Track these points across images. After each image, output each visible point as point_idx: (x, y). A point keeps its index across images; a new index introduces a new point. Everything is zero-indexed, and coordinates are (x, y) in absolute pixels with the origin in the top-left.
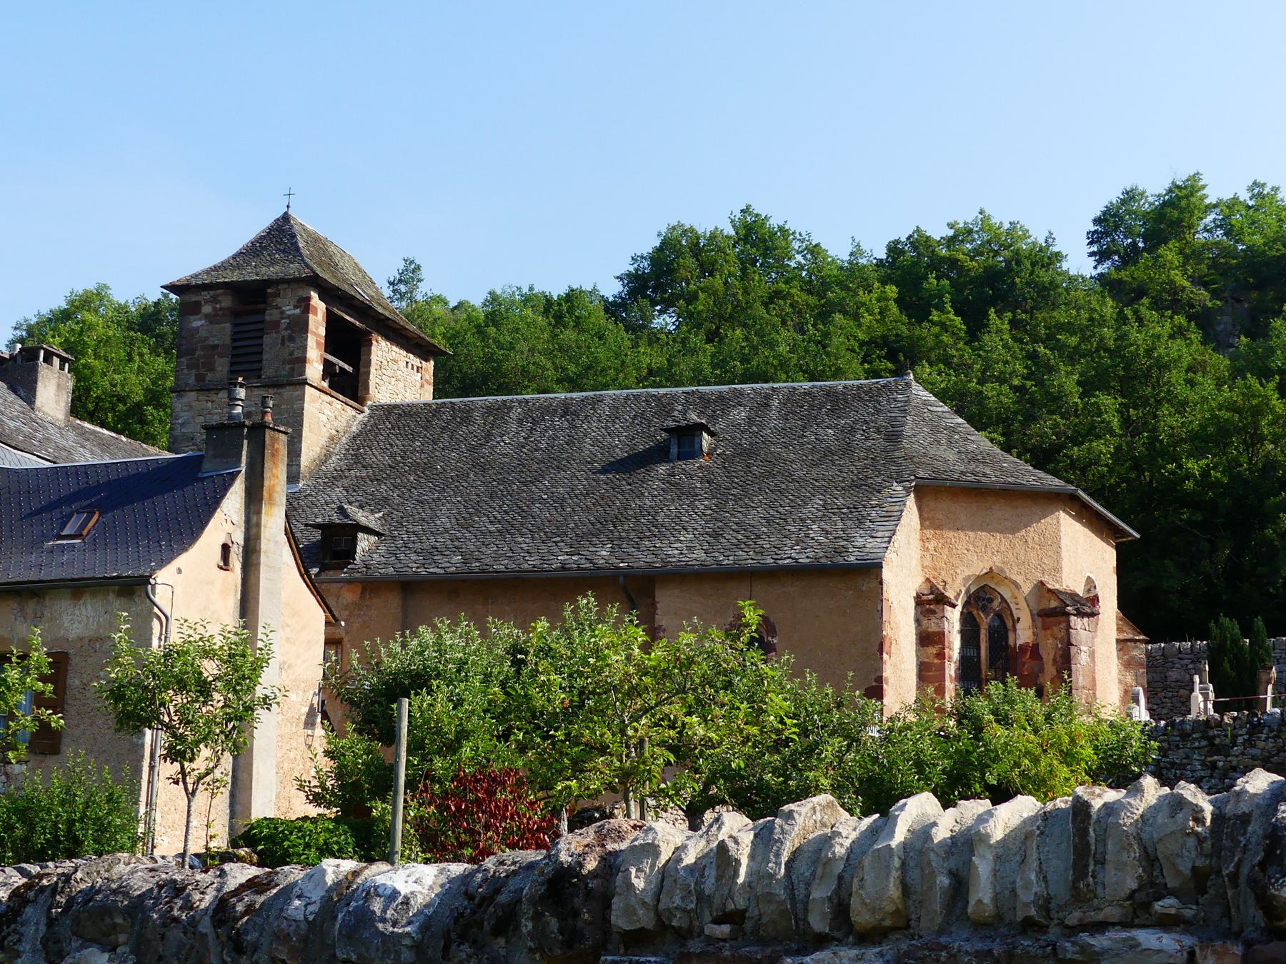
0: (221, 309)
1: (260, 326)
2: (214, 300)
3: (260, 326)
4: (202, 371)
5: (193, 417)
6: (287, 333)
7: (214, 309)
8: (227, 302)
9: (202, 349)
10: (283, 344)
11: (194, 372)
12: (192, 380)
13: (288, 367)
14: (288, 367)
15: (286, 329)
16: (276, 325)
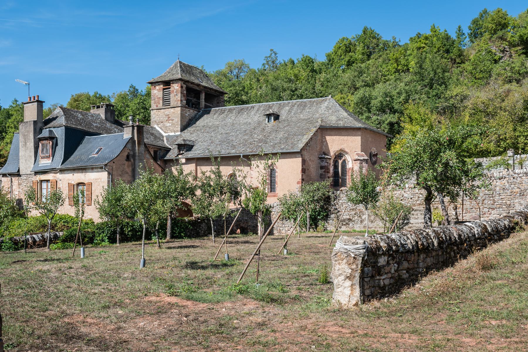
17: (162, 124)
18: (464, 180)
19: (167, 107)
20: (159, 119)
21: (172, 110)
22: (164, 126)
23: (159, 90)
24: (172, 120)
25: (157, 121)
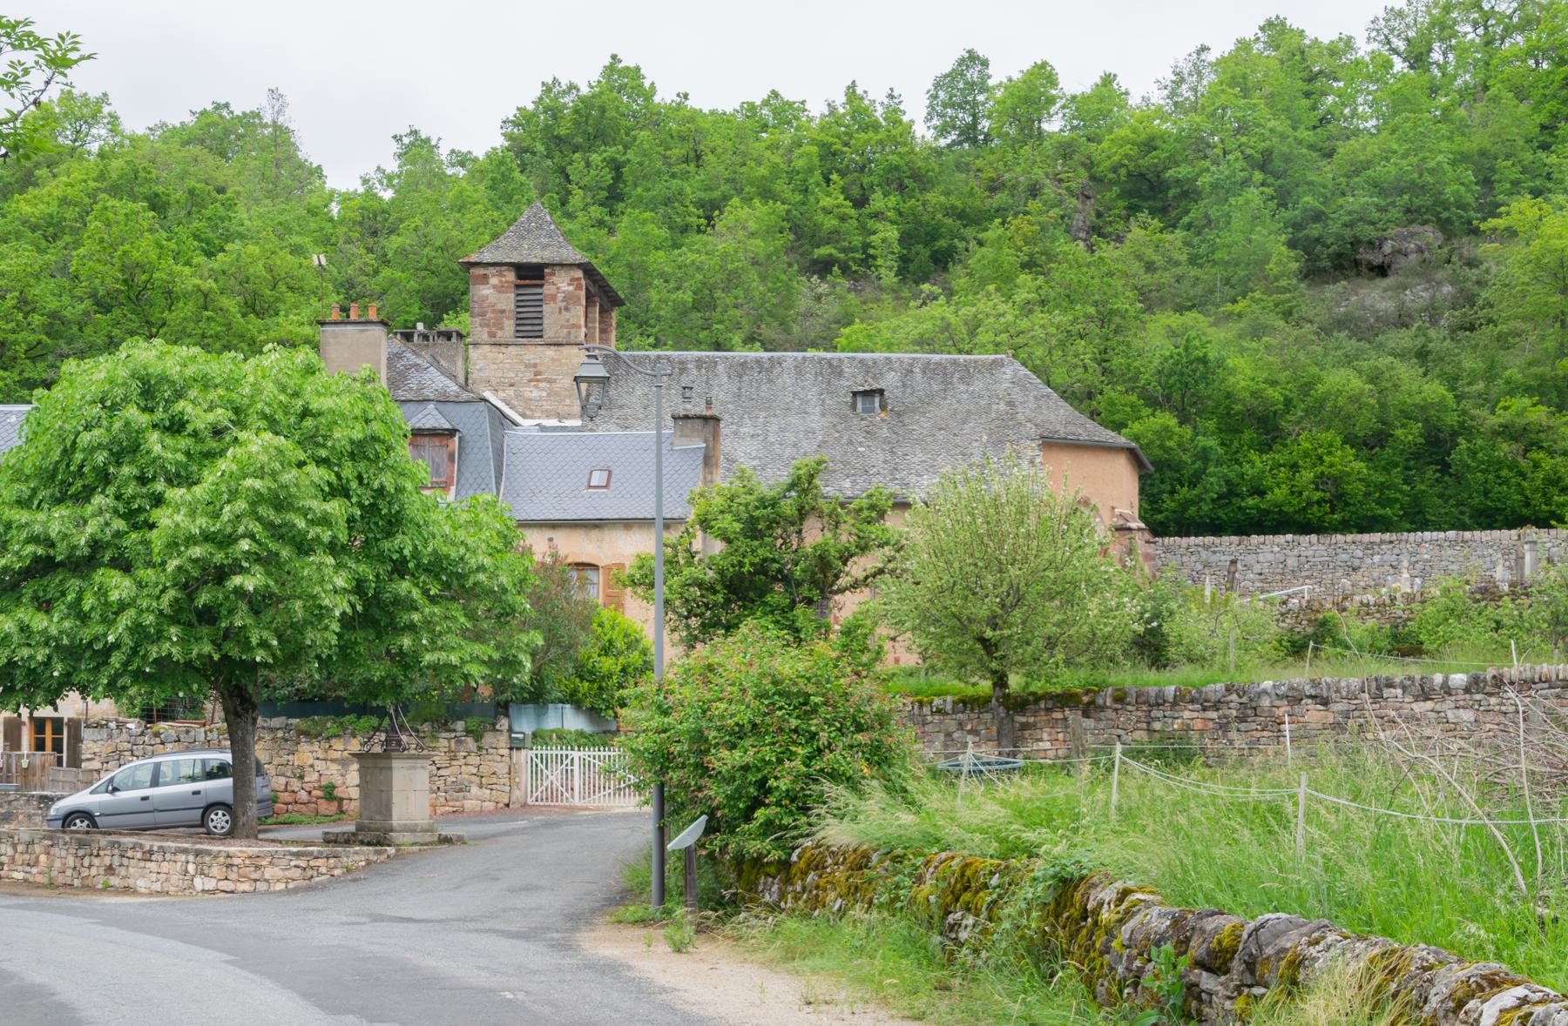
2: (500, 274)
8: (511, 276)
12: (485, 337)
16: (553, 298)
17: (511, 392)
21: (551, 352)
22: (518, 396)
23: (500, 289)
24: (549, 381)
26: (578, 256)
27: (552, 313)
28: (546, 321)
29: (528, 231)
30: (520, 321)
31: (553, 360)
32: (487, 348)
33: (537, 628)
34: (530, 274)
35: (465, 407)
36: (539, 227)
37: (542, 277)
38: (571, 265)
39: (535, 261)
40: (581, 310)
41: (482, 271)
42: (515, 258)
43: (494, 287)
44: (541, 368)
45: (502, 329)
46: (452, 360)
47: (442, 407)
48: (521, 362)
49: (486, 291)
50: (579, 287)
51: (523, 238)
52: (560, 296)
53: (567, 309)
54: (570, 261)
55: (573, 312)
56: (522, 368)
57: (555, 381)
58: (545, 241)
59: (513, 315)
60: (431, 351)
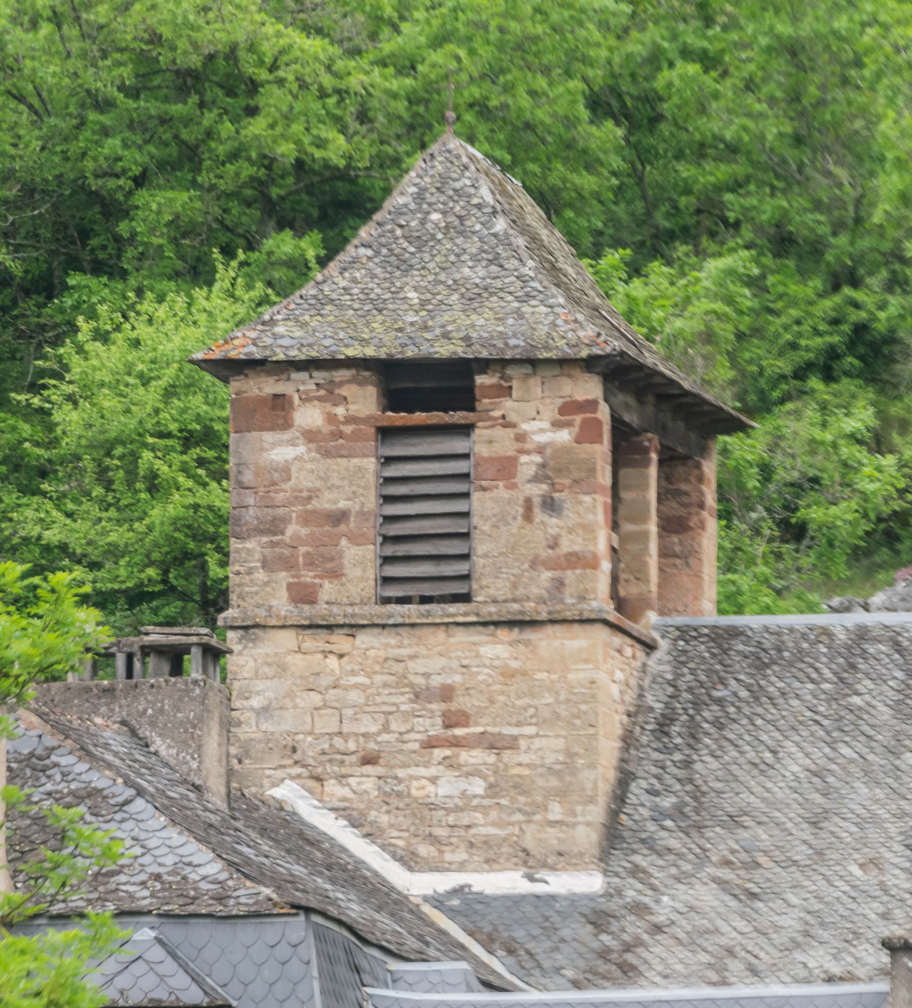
0: (350, 420)
1: (459, 467)
2: (330, 394)
3: (459, 467)
4: (308, 577)
5: (291, 695)
6: (537, 491)
7: (331, 418)
8: (364, 401)
9: (307, 519)
10: (528, 516)
11: (284, 577)
12: (281, 603)
13: (546, 576)
14: (546, 576)
15: (535, 479)
16: (506, 468)
17: (366, 782)
18: (714, 74)
19: (412, 611)
20: (327, 723)
21: (496, 649)
22: (393, 797)
23: (328, 443)
24: (495, 744)
25: (310, 748)
26: (584, 335)
27: (502, 519)
28: (481, 547)
29: (420, 241)
30: (395, 544)
31: (508, 674)
32: (288, 639)
33: (647, 431)
34: (430, 393)
35: (246, 932)
36: (457, 228)
37: (465, 398)
38: (564, 363)
39: (443, 350)
40: (594, 508)
41: (269, 386)
42: (380, 340)
43: (311, 436)
44: (461, 702)
45: (335, 574)
46: (190, 740)
47: (175, 933)
48: (402, 680)
49: (280, 450)
50: (589, 433)
51: (404, 266)
52: (529, 463)
53: (550, 505)
54: (560, 348)
55: (571, 516)
56: (404, 702)
57: (512, 744)
58: (474, 274)
59: (371, 528)
60: (120, 711)
